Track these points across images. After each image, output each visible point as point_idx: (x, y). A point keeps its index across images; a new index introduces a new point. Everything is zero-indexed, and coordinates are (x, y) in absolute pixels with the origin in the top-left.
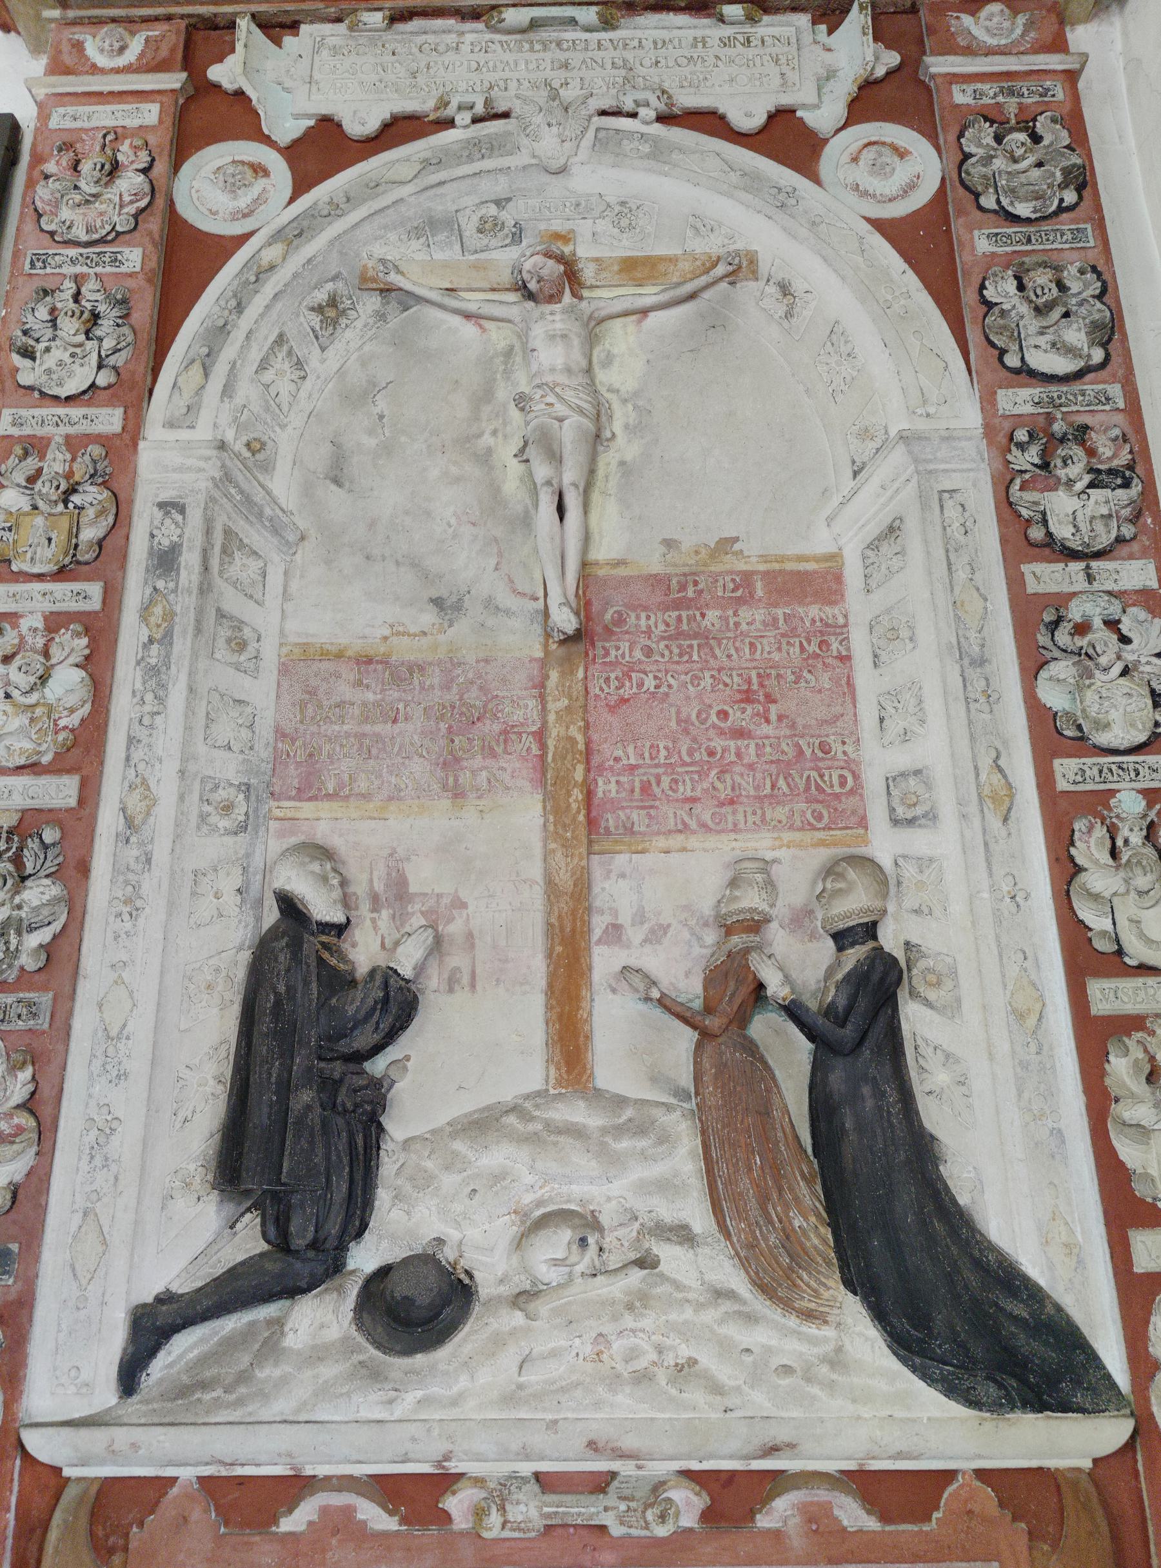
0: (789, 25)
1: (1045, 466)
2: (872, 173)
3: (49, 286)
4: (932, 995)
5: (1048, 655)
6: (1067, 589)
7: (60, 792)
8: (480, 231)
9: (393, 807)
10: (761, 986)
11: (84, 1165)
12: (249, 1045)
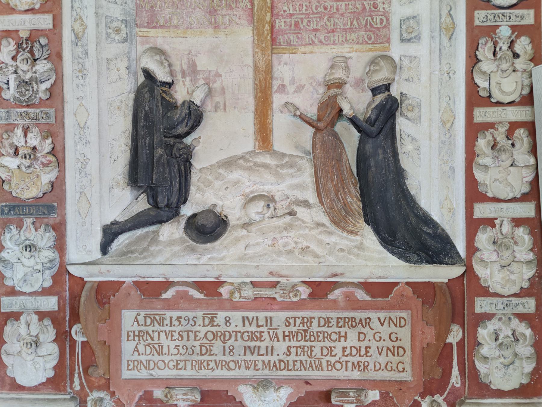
4: (409, 115)
7: (45, 22)
9: (189, 32)
10: (341, 110)
12: (136, 131)
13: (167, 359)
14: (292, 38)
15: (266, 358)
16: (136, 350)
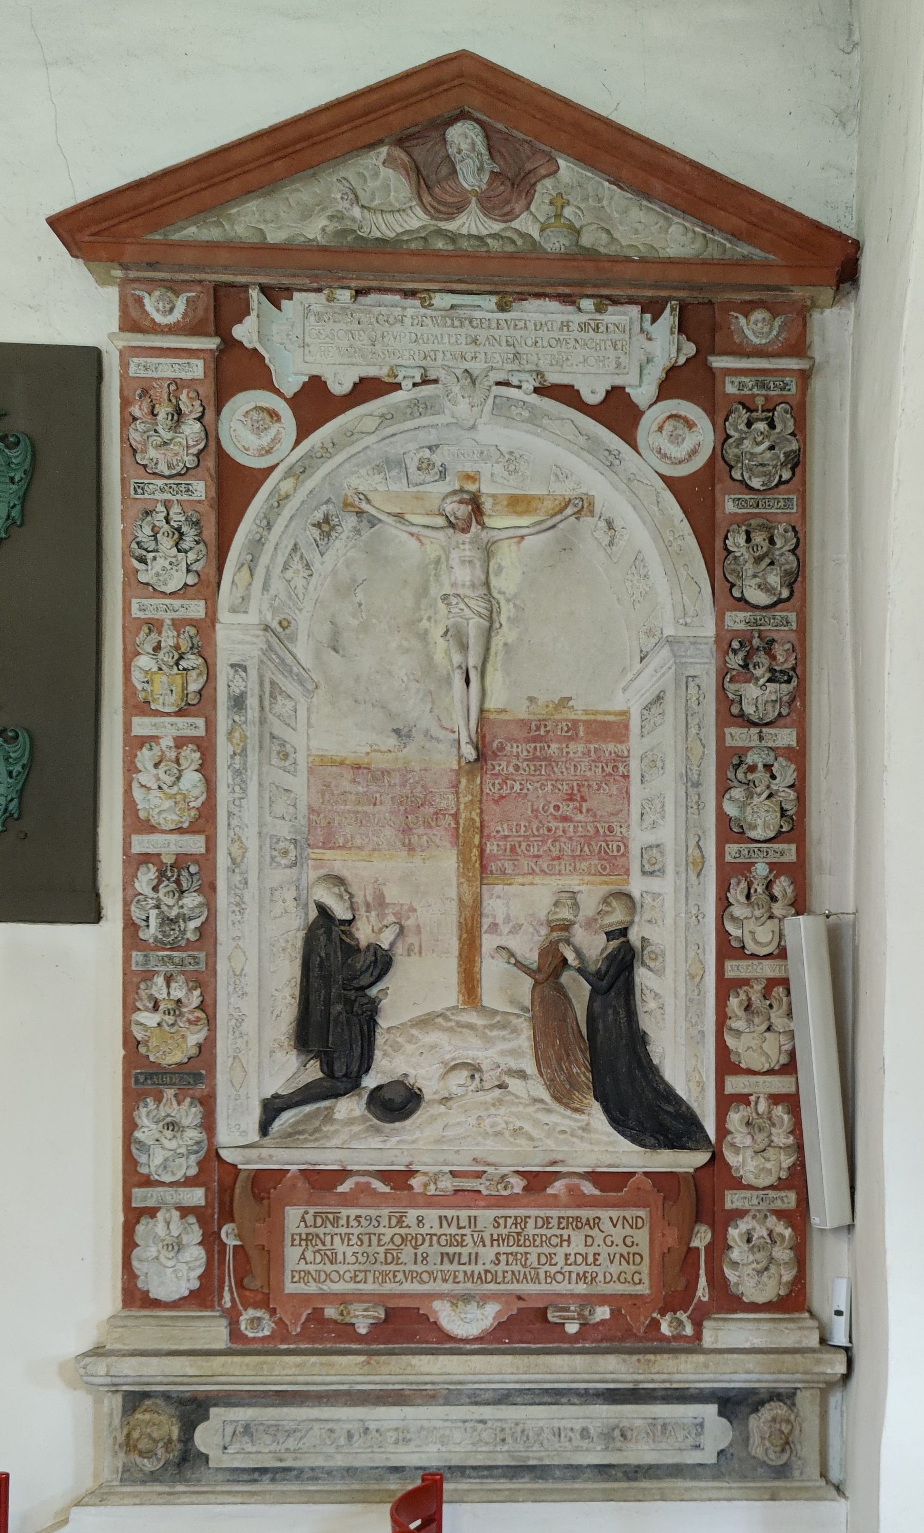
0: (625, 314)
1: (745, 666)
2: (672, 442)
4: (652, 964)
5: (732, 784)
6: (747, 744)
7: (195, 844)
8: (419, 469)
9: (376, 854)
11: (231, 1036)
12: (308, 981)
13: (342, 1268)
16: (303, 1257)
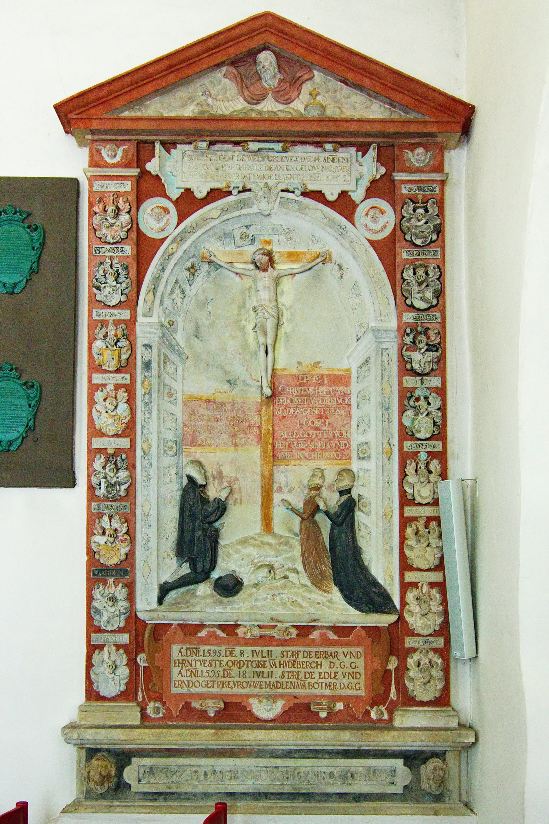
1: (414, 342)
2: (372, 221)
3: (102, 261)
4: (364, 509)
5: (407, 408)
7: (124, 443)
8: (241, 238)
10: (318, 506)
12: (183, 518)
13: (201, 680)
14: (286, 455)
15: (267, 680)
16: (180, 673)
